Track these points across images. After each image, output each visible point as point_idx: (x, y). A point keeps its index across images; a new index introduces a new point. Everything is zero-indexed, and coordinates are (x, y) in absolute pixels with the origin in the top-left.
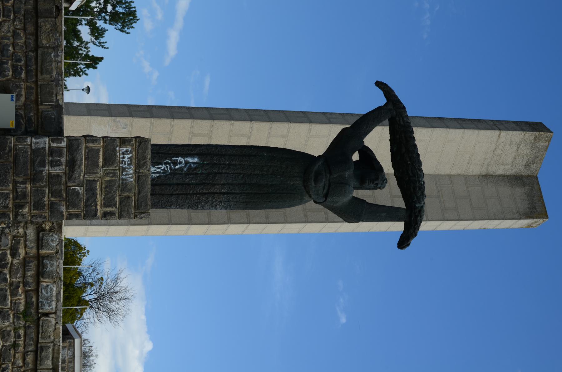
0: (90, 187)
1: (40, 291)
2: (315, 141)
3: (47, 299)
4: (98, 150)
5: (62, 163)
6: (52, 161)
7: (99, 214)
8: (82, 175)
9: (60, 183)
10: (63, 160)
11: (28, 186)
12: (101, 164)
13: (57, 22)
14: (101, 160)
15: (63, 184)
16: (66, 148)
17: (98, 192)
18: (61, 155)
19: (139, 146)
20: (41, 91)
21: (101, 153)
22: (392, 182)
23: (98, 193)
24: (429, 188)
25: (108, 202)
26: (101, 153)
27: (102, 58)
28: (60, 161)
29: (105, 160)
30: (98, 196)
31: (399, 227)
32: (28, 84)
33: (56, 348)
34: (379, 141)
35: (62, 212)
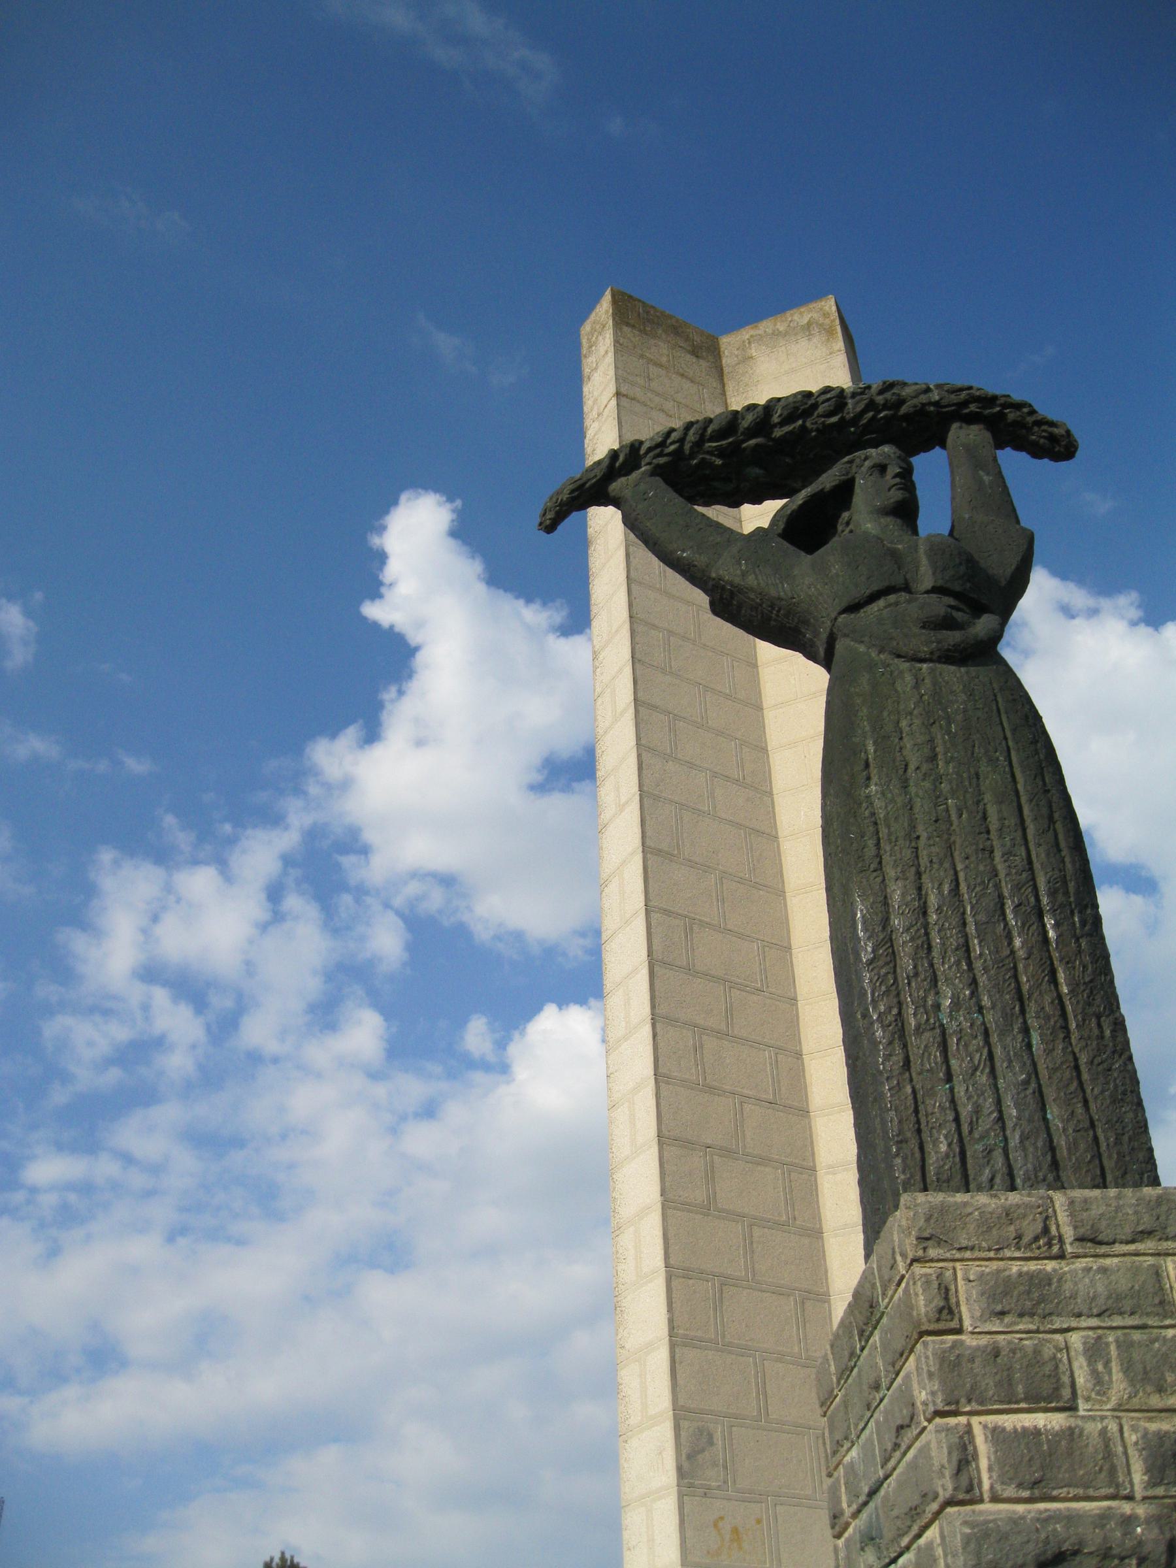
4: (996, 1434)
8: (1126, 1508)
14: (1040, 1420)
19: (940, 1242)
21: (1009, 1422)
26: (1009, 1422)
29: (1038, 1401)
31: (1012, 461)
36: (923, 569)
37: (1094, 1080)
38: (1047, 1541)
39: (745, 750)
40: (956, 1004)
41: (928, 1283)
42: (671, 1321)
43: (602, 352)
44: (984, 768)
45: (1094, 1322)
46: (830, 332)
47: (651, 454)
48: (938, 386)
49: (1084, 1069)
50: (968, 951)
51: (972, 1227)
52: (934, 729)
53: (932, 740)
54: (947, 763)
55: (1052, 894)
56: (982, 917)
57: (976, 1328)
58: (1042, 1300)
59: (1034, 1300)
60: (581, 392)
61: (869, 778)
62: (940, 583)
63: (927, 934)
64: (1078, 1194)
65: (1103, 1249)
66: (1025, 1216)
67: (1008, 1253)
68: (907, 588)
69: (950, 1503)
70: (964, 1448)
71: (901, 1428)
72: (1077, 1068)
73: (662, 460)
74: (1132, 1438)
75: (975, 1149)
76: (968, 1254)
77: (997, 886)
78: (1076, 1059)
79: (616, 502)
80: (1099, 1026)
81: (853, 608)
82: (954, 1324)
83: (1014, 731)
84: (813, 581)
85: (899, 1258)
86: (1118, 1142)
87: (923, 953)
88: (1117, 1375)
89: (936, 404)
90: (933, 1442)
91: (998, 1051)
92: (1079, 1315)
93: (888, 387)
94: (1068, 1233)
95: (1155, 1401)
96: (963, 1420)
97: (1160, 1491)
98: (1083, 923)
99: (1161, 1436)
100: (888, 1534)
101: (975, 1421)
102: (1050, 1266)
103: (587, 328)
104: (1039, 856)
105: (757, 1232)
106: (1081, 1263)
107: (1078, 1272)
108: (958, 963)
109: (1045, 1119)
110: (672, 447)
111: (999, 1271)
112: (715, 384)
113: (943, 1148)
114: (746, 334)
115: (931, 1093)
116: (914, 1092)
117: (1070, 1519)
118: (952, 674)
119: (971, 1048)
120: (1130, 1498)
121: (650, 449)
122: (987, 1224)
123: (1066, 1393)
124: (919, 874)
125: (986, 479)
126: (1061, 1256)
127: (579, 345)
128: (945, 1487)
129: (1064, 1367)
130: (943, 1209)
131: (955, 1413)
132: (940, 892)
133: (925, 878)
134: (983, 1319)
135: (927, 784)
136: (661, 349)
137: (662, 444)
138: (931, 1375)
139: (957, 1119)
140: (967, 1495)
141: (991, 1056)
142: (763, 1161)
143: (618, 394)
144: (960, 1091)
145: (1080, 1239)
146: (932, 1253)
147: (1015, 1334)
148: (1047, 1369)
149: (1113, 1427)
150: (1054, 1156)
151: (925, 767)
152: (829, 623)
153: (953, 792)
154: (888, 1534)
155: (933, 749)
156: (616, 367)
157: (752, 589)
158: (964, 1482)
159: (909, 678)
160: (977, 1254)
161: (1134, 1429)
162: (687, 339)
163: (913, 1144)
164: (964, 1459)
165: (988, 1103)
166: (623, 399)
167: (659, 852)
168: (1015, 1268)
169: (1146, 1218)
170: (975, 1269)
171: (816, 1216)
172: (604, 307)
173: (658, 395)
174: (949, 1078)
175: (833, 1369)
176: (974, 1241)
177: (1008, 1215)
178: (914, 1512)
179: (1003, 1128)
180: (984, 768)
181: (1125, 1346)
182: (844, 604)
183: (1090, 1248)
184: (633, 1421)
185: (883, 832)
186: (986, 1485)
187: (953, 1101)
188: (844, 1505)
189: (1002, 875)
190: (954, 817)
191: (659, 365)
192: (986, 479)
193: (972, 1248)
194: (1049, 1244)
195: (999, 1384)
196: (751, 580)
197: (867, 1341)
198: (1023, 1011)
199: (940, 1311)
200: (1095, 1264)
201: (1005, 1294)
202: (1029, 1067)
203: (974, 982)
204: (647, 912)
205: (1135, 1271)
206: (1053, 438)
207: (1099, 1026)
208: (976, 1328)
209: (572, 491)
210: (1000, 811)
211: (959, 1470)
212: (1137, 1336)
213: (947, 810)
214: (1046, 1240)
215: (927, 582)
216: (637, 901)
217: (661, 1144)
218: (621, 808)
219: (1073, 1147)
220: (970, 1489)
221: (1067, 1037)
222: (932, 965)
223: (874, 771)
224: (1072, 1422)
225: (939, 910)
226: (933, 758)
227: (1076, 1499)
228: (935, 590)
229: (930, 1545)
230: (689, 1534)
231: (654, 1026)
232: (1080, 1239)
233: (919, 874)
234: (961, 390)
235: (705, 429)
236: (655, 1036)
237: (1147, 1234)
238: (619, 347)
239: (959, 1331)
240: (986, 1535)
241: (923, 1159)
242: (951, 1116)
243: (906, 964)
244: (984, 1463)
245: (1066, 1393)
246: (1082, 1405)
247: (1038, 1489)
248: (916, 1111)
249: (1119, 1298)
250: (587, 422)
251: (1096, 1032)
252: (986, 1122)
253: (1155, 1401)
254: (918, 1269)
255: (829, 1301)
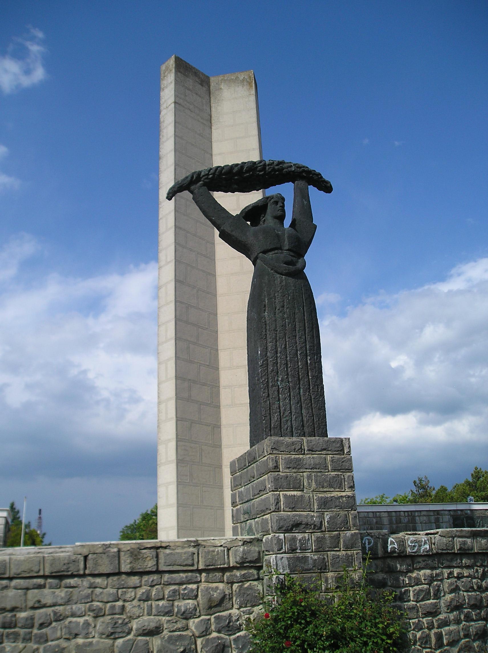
0: (325, 504)
1: (413, 554)
2: (234, 273)
3: (420, 546)
4: (285, 496)
5: (302, 537)
6: (301, 549)
7: (349, 494)
8: (312, 514)
9: (323, 538)
10: (299, 536)
11: (330, 575)
12: (299, 493)
13: (125, 549)
14: (295, 493)
15: (324, 534)
16: (285, 533)
17: (329, 495)
18: (294, 539)
19: (276, 449)
20: (212, 565)
21: (289, 493)
22: (273, 191)
23: (330, 495)
24: (274, 156)
25: (340, 487)
26: (289, 493)
27: (29, 523)
28: (300, 540)
29: (295, 489)
30: (332, 495)
31: (312, 189)
32: (203, 580)
33: (458, 534)
34: (234, 203)
35: (352, 535)
36: (286, 242)
37: (315, 403)
38: (294, 521)
39: (208, 244)
40: (282, 380)
41: (273, 460)
42: (177, 434)
43: (169, 82)
44: (297, 311)
45: (310, 470)
46: (250, 84)
47: (204, 177)
48: (295, 165)
49: (313, 400)
50: (287, 365)
51: (284, 446)
52: (284, 298)
53: (283, 301)
54: (287, 308)
55: (310, 350)
56: (291, 356)
57: (283, 472)
58: (299, 465)
59: (296, 465)
60: (160, 94)
61: (265, 310)
62: (290, 248)
63: (277, 359)
64: (309, 438)
65: (313, 453)
66: (297, 444)
67: (292, 453)
68: (280, 248)
69: (273, 512)
70: (278, 499)
71: (260, 491)
72: (311, 399)
73: (207, 180)
74: (315, 498)
75: (283, 420)
76: (282, 453)
77: (296, 347)
78: (311, 397)
79: (192, 192)
80: (318, 388)
81: (265, 252)
82: (278, 470)
83: (305, 300)
84: (250, 233)
85: (265, 451)
86: (319, 420)
87: (275, 365)
88: (314, 483)
89: (293, 171)
90: (270, 495)
91: (292, 394)
92: (307, 469)
93: (280, 163)
94: (306, 448)
95: (321, 490)
96: (278, 492)
97: (320, 510)
98: (317, 359)
99: (322, 497)
100: (253, 513)
101: (281, 493)
102: (301, 456)
103: (163, 67)
104: (308, 338)
105: (202, 407)
106: (308, 456)
107: (308, 458)
108: (284, 368)
109: (302, 413)
110: (211, 176)
111: (289, 457)
112: (208, 97)
113: (276, 418)
114: (221, 78)
115: (274, 404)
116: (270, 403)
117: (300, 516)
118: (291, 280)
119: (286, 392)
120: (314, 512)
121: (203, 176)
122: (288, 445)
123: (302, 487)
124: (276, 342)
125: (305, 203)
126: (304, 454)
127: (160, 74)
128: (273, 508)
129: (302, 481)
130: (278, 442)
131: (276, 491)
132: (281, 348)
133: (278, 343)
134: (285, 469)
135: (281, 314)
136: (190, 82)
137: (208, 175)
138: (272, 482)
139: (280, 412)
140: (278, 510)
141: (290, 394)
142: (204, 384)
143: (175, 103)
144: (281, 404)
145: (309, 450)
146: (274, 452)
147: (292, 473)
148: (298, 481)
149: (311, 495)
150: (303, 423)
151: (281, 309)
152: (256, 254)
153: (288, 318)
154: (253, 513)
155: (283, 304)
156: (175, 91)
157: (234, 236)
158: (277, 507)
159: (279, 280)
160: (284, 453)
161: (316, 496)
162: (199, 78)
163: (268, 417)
164: (278, 502)
165: (288, 406)
166: (177, 104)
167: (180, 282)
168: (293, 456)
169: (324, 446)
170: (284, 456)
171: (219, 402)
172: (171, 62)
173: (188, 102)
174: (279, 400)
175: (237, 465)
176: (284, 449)
177: (293, 443)
178: (263, 511)
179: (291, 415)
180: (297, 311)
181: (316, 476)
182: (262, 250)
183: (311, 452)
184: (162, 461)
185: (268, 328)
186: (282, 508)
187: (279, 407)
188: (237, 500)
189: (298, 343)
190: (287, 326)
191: (189, 89)
192: (305, 203)
193: (283, 451)
194: (302, 451)
195: (287, 485)
196: (233, 233)
197: (251, 465)
198: (299, 383)
199: (275, 467)
200: (311, 456)
201: (290, 463)
202: (299, 399)
203: (288, 374)
204: (175, 302)
205: (321, 458)
206: (326, 186)
207: (318, 388)
208: (283, 472)
209: (178, 188)
210: (299, 325)
211: (277, 504)
212: (319, 474)
213: (285, 323)
214: (301, 451)
215: (287, 247)
216: (172, 297)
217: (176, 379)
218: (168, 263)
219: (307, 422)
220: (278, 509)
221: (309, 392)
222: (277, 368)
223: (267, 308)
224: (302, 494)
225: (280, 353)
226: (283, 307)
227: (302, 511)
228: (288, 250)
229: (267, 519)
230: (179, 495)
231: (176, 341)
232: (309, 450)
233: (276, 342)
234: (301, 167)
235: (221, 171)
236: (176, 344)
237: (324, 449)
238: (177, 82)
239: (279, 471)
240: (282, 519)
241: (270, 422)
242: (278, 411)
243: (270, 368)
244: (282, 503)
245: (302, 487)
246: (305, 490)
247: (293, 509)
248: (270, 409)
249: (316, 465)
250: (162, 108)
251: (317, 390)
252: (287, 413)
253: (321, 490)
254: (271, 456)
255: (220, 428)
